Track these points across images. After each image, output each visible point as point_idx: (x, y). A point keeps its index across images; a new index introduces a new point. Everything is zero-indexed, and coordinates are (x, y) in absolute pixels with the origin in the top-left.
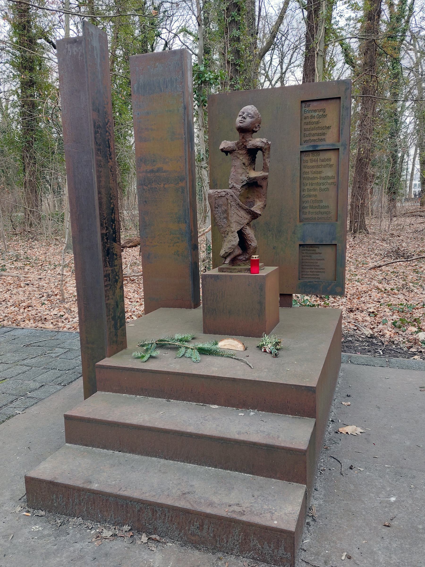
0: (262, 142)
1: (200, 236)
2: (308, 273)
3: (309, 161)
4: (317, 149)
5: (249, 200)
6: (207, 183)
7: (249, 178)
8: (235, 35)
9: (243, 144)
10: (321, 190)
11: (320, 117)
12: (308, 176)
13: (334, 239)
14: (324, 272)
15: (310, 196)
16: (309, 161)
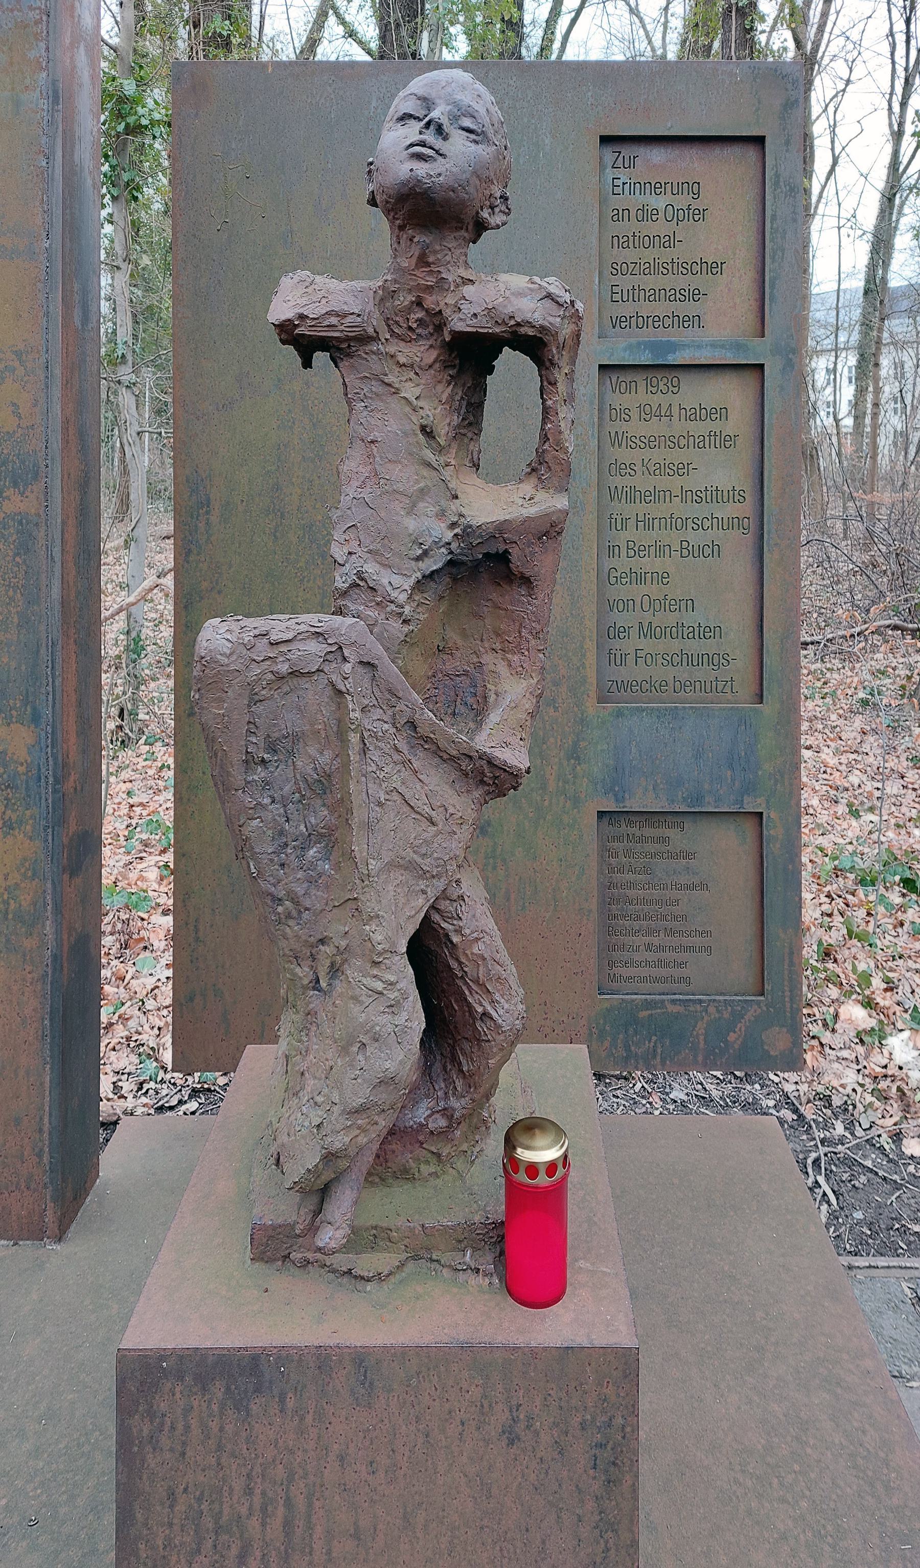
0: (549, 296)
1: (107, 619)
2: (637, 957)
3: (635, 414)
4: (671, 359)
5: (451, 665)
6: (134, 434)
7: (467, 533)
8: (218, 30)
9: (419, 303)
10: (688, 551)
11: (678, 216)
12: (628, 481)
13: (749, 788)
14: (709, 949)
15: (640, 578)
16: (635, 414)
